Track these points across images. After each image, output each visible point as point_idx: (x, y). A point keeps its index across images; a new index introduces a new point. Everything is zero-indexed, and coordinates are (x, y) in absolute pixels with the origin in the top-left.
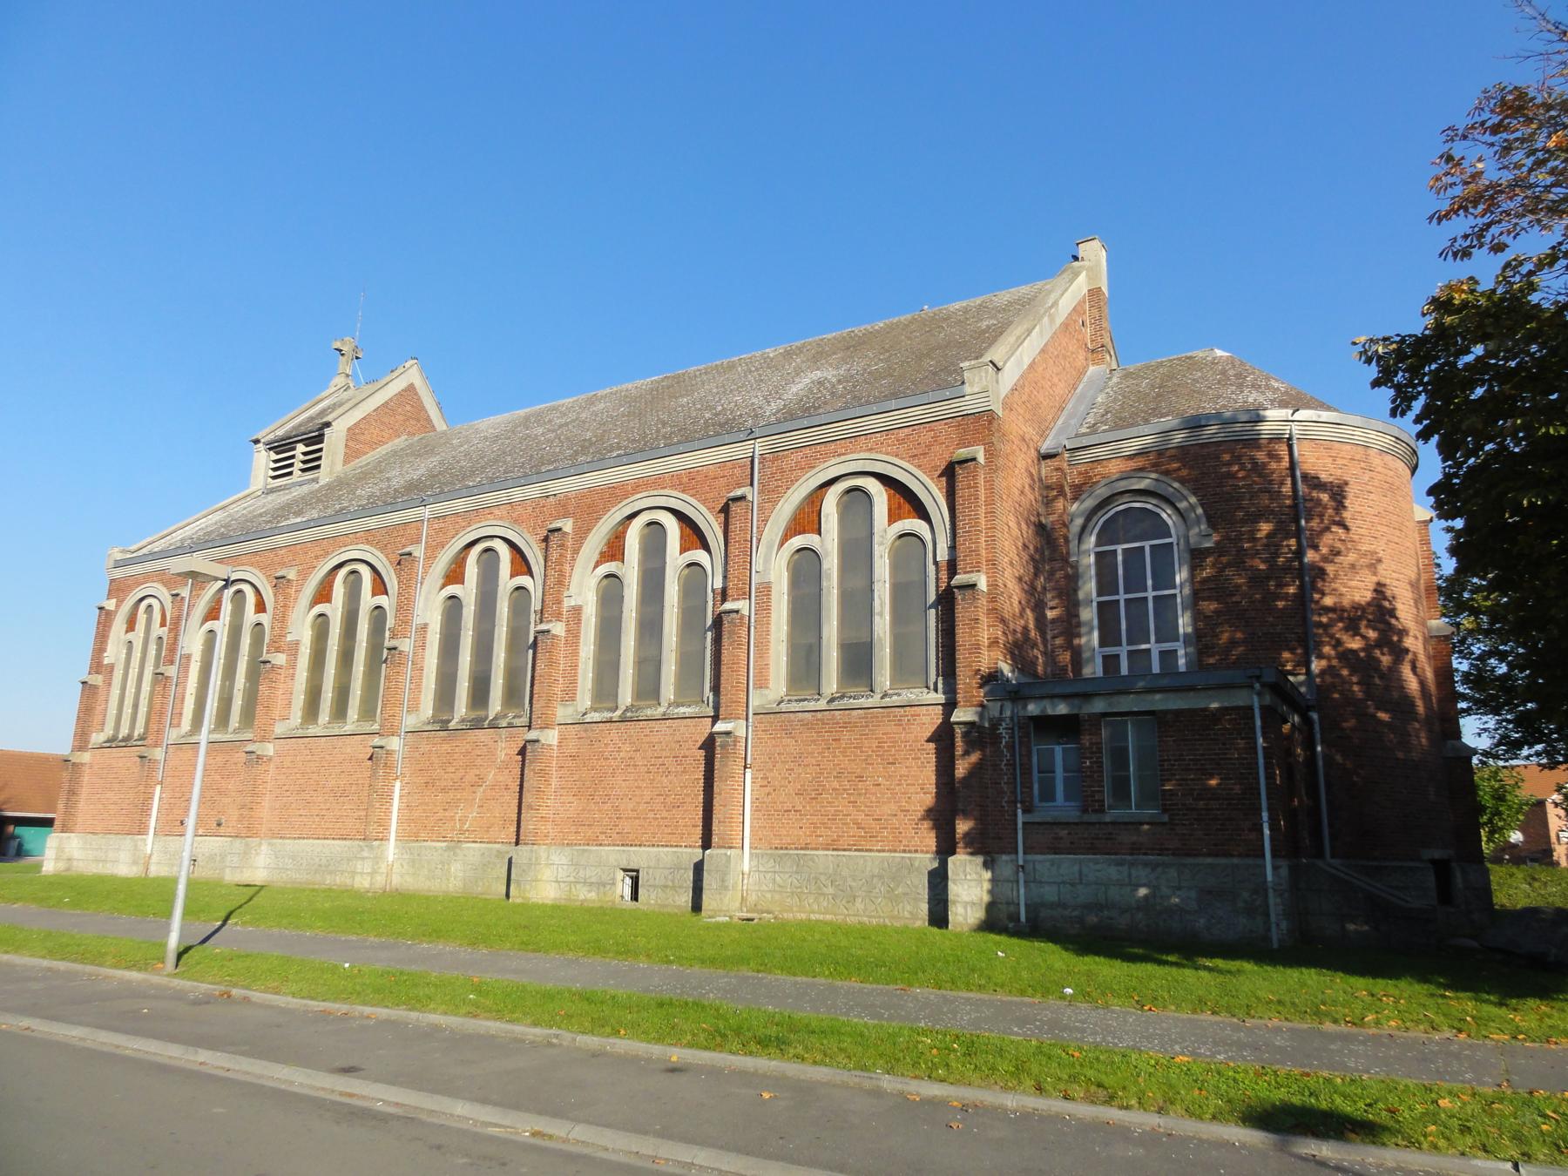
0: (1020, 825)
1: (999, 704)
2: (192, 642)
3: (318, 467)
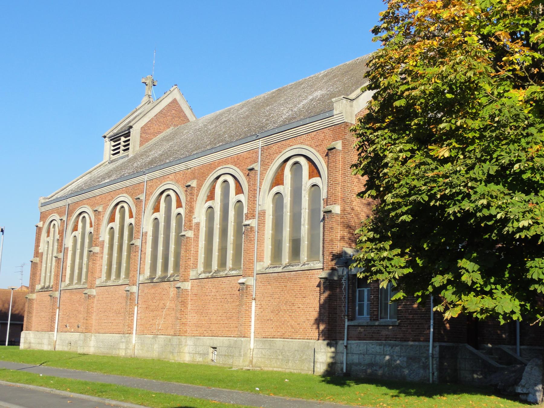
0: (346, 327)
1: (342, 268)
2: (69, 243)
3: (128, 149)
